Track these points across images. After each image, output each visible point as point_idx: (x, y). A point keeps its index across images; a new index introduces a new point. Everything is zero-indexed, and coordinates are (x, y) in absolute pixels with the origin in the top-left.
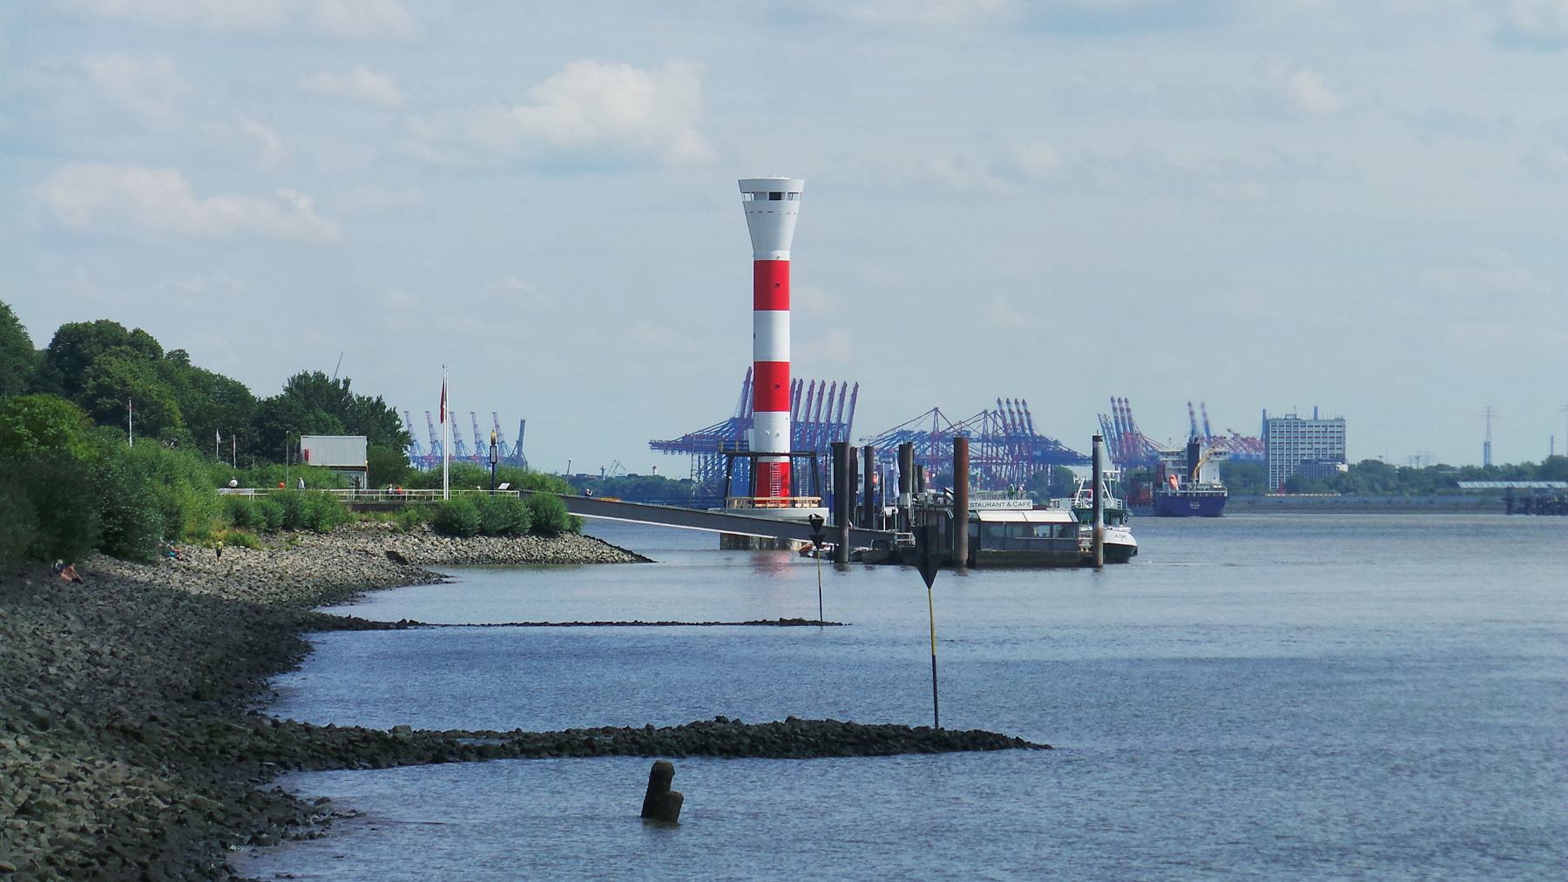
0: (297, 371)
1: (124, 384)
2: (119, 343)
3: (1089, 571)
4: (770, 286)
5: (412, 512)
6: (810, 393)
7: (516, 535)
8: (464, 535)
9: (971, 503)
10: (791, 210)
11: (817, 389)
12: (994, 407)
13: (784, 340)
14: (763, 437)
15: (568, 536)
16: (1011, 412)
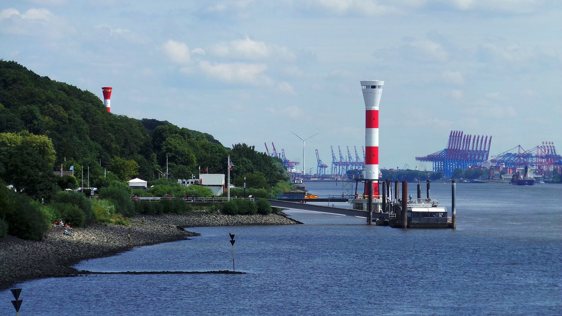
0: (241, 141)
1: (176, 148)
2: (176, 132)
3: (451, 230)
4: (371, 119)
5: (214, 206)
6: (474, 140)
7: (252, 214)
8: (232, 214)
9: (408, 205)
10: (379, 93)
11: (476, 139)
12: (541, 145)
13: (376, 138)
14: (369, 174)
15: (271, 215)
16: (547, 147)
